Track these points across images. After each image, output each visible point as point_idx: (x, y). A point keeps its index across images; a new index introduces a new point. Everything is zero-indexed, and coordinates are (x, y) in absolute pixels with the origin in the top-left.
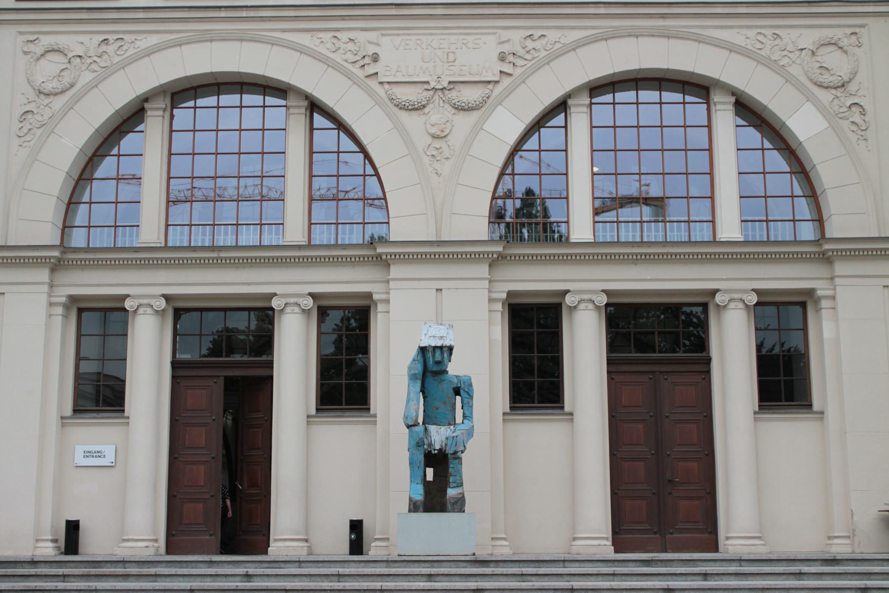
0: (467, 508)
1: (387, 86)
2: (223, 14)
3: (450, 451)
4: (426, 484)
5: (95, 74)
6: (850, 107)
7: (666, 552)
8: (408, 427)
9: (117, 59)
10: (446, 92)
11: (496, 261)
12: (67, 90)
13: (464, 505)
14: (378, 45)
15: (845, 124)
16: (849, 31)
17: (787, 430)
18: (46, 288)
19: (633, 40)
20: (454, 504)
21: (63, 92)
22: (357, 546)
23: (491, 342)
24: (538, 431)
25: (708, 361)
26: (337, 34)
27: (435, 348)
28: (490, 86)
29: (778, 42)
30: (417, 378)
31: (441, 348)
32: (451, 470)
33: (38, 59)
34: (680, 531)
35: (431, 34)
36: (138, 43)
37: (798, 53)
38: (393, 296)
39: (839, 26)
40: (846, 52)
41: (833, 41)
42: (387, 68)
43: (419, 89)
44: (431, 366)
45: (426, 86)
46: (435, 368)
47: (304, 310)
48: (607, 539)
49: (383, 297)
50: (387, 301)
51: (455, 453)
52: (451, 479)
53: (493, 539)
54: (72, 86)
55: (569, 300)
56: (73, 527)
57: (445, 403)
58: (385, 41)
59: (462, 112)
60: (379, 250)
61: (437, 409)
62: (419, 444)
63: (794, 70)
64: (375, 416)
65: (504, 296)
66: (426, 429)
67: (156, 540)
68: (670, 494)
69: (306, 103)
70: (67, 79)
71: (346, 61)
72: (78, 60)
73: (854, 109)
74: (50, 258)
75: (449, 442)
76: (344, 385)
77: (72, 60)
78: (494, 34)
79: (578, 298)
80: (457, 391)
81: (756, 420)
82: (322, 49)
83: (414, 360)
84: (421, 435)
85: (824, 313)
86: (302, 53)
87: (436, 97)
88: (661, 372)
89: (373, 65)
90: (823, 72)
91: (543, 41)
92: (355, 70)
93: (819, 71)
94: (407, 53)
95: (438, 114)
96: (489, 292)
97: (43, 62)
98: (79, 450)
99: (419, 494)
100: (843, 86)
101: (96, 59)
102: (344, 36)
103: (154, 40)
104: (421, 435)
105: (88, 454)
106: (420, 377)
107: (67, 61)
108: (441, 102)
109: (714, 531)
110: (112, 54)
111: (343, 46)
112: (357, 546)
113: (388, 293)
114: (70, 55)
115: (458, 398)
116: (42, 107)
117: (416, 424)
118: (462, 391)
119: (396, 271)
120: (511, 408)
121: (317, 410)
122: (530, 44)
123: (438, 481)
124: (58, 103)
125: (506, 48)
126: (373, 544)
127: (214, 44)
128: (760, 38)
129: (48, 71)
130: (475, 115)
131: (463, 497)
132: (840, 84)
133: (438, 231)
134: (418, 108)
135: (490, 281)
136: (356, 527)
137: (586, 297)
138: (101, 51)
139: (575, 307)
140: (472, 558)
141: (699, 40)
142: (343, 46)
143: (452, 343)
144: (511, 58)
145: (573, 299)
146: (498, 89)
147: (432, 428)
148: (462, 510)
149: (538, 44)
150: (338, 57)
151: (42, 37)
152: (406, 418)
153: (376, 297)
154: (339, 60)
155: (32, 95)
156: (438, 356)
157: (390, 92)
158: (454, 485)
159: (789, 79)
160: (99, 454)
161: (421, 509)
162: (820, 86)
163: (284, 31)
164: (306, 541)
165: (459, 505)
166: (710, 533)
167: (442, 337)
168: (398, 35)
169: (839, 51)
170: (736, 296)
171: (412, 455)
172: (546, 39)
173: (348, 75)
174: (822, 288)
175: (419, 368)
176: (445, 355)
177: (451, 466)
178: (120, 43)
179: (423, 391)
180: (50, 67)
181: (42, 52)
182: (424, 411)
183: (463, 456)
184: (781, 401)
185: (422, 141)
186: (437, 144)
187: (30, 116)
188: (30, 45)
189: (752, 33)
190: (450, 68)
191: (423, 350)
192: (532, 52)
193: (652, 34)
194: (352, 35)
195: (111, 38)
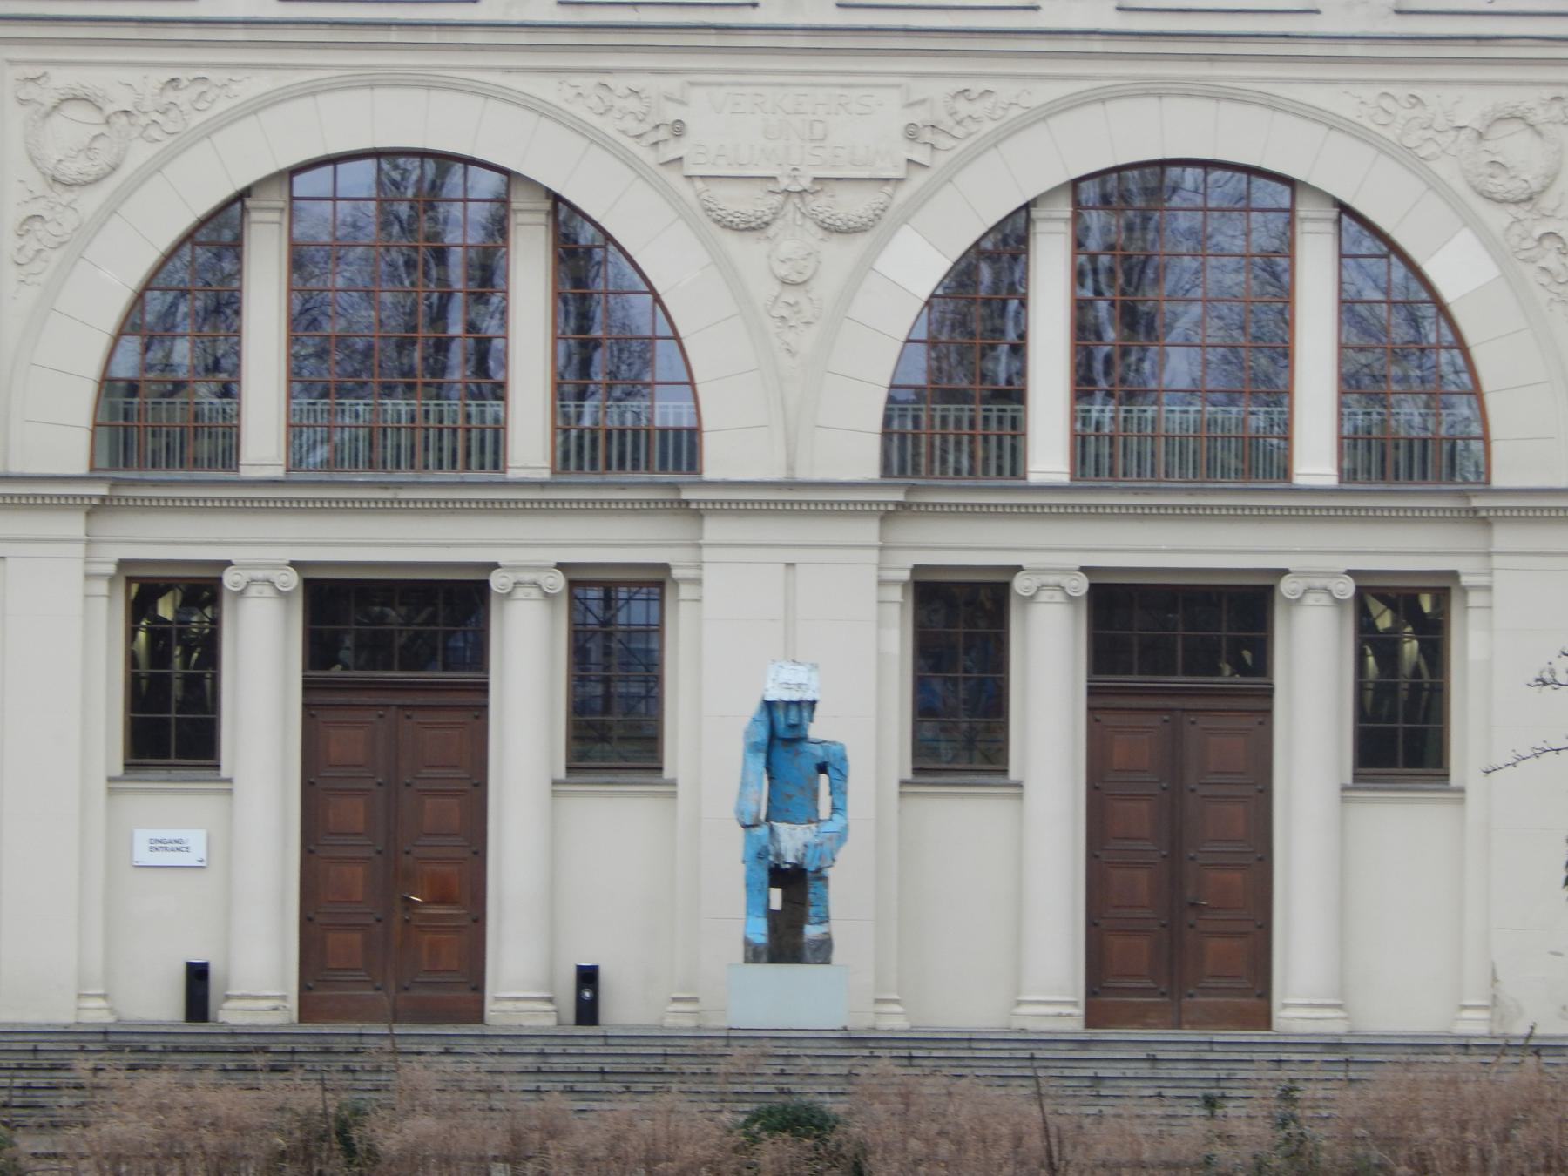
1: (699, 184)
2: (394, 36)
3: (811, 867)
4: (772, 916)
5: (157, 147)
6: (1541, 239)
7: (1180, 1027)
8: (745, 827)
9: (197, 119)
10: (809, 198)
12: (106, 176)
14: (682, 103)
15: (1530, 271)
16: (1548, 93)
17: (1400, 818)
18: (80, 549)
19: (1153, 101)
21: (97, 180)
22: (587, 1012)
23: (881, 656)
24: (961, 816)
25: (1268, 694)
26: (607, 79)
27: (789, 704)
28: (888, 189)
29: (1417, 111)
30: (759, 750)
31: (799, 704)
32: (811, 896)
33: (48, 115)
34: (1206, 991)
35: (782, 85)
36: (235, 87)
37: (1453, 133)
39: (1533, 84)
40: (1539, 134)
41: (1518, 114)
42: (702, 150)
43: (756, 190)
44: (783, 735)
45: (771, 186)
46: (789, 735)
47: (546, 595)
48: (1074, 1004)
49: (691, 573)
50: (698, 582)
51: (819, 870)
52: (812, 910)
53: (878, 1001)
54: (114, 169)
56: (588, 977)
57: (802, 788)
58: (697, 94)
59: (836, 236)
61: (790, 797)
62: (761, 855)
63: (1442, 168)
64: (673, 783)
66: (772, 829)
67: (283, 998)
68: (1192, 926)
69: (547, 205)
70: (103, 160)
71: (624, 132)
72: (124, 119)
73: (1547, 243)
74: (90, 497)
76: (615, 723)
77: (113, 119)
78: (898, 86)
80: (822, 768)
81: (1344, 800)
82: (579, 110)
83: (755, 720)
84: (765, 841)
85: (1473, 615)
86: (542, 114)
87: (790, 207)
88: (1184, 710)
89: (672, 143)
90: (1497, 171)
91: (988, 102)
92: (641, 150)
93: (1489, 171)
94: (739, 119)
95: (793, 241)
97: (56, 120)
98: (142, 837)
99: (759, 932)
100: (1530, 199)
101: (156, 116)
102: (619, 84)
103: (262, 83)
104: (765, 841)
105: (157, 845)
106: (764, 748)
107: (102, 120)
108: (798, 216)
109: (1265, 993)
110: (186, 107)
111: (619, 103)
112: (587, 1012)
113: (700, 567)
114: (109, 109)
115: (824, 778)
116: (59, 208)
118: (830, 769)
121: (569, 769)
122: (963, 107)
123: (791, 919)
124: (91, 201)
125: (920, 116)
127: (378, 92)
128: (1386, 103)
129: (67, 136)
130: (860, 243)
132: (1523, 197)
133: (791, 467)
134: (756, 227)
136: (197, 975)
137: (1051, 579)
138: (165, 100)
140: (844, 1034)
141: (1273, 104)
142: (619, 103)
144: (927, 135)
145: (1027, 583)
146: (903, 194)
147: (782, 828)
148: (826, 961)
149: (978, 108)
150: (608, 126)
151: (52, 71)
152: (740, 813)
153: (677, 573)
154: (610, 131)
155: (39, 186)
156: (793, 717)
157: (705, 196)
159: (1435, 185)
160: (178, 846)
161: (765, 958)
162: (1490, 197)
163: (508, 70)
165: (823, 951)
166: (1259, 996)
167: (799, 685)
168: (720, 85)
169: (1528, 133)
170: (1317, 582)
171: (750, 870)
172: (992, 99)
173: (629, 161)
174: (1469, 570)
175: (762, 734)
178: (201, 88)
179: (769, 767)
180: (72, 128)
181: (55, 101)
182: (770, 800)
183: (831, 873)
184: (1395, 766)
185: (764, 289)
186: (790, 296)
187: (37, 225)
188: (31, 87)
189: (1370, 94)
190: (816, 152)
191: (769, 706)
192: (968, 122)
193: (1189, 91)
194: (636, 82)
195: (184, 75)
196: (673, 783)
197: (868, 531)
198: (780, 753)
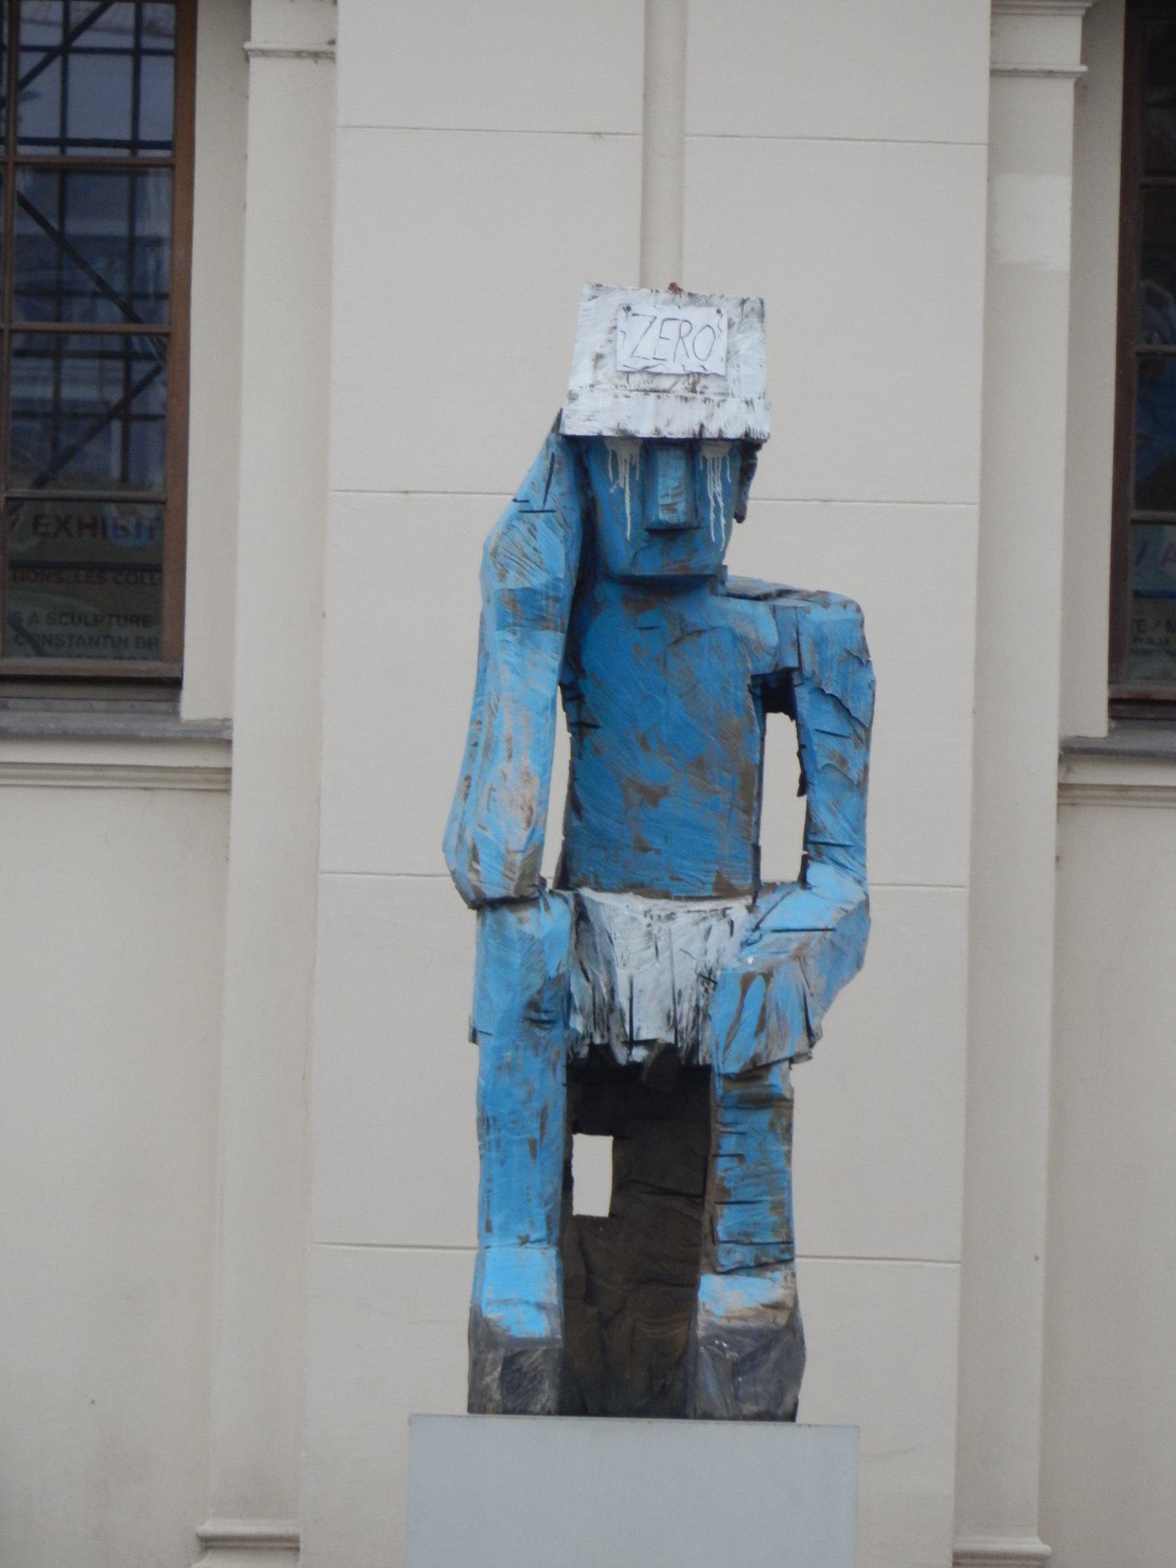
0: (814, 1391)
4: (575, 1238)
44: (630, 562)
52: (727, 1221)
62: (542, 1011)
64: (218, 737)
80: (775, 692)
106: (560, 611)
115: (779, 726)
120: (1125, 708)
133: (501, 924)
147: (620, 912)
158: (741, 1254)
161: (547, 1393)
165: (765, 1375)
171: (499, 1069)
175: (552, 560)
176: (715, 488)
177: (729, 1144)
183: (801, 1082)
191: (580, 456)
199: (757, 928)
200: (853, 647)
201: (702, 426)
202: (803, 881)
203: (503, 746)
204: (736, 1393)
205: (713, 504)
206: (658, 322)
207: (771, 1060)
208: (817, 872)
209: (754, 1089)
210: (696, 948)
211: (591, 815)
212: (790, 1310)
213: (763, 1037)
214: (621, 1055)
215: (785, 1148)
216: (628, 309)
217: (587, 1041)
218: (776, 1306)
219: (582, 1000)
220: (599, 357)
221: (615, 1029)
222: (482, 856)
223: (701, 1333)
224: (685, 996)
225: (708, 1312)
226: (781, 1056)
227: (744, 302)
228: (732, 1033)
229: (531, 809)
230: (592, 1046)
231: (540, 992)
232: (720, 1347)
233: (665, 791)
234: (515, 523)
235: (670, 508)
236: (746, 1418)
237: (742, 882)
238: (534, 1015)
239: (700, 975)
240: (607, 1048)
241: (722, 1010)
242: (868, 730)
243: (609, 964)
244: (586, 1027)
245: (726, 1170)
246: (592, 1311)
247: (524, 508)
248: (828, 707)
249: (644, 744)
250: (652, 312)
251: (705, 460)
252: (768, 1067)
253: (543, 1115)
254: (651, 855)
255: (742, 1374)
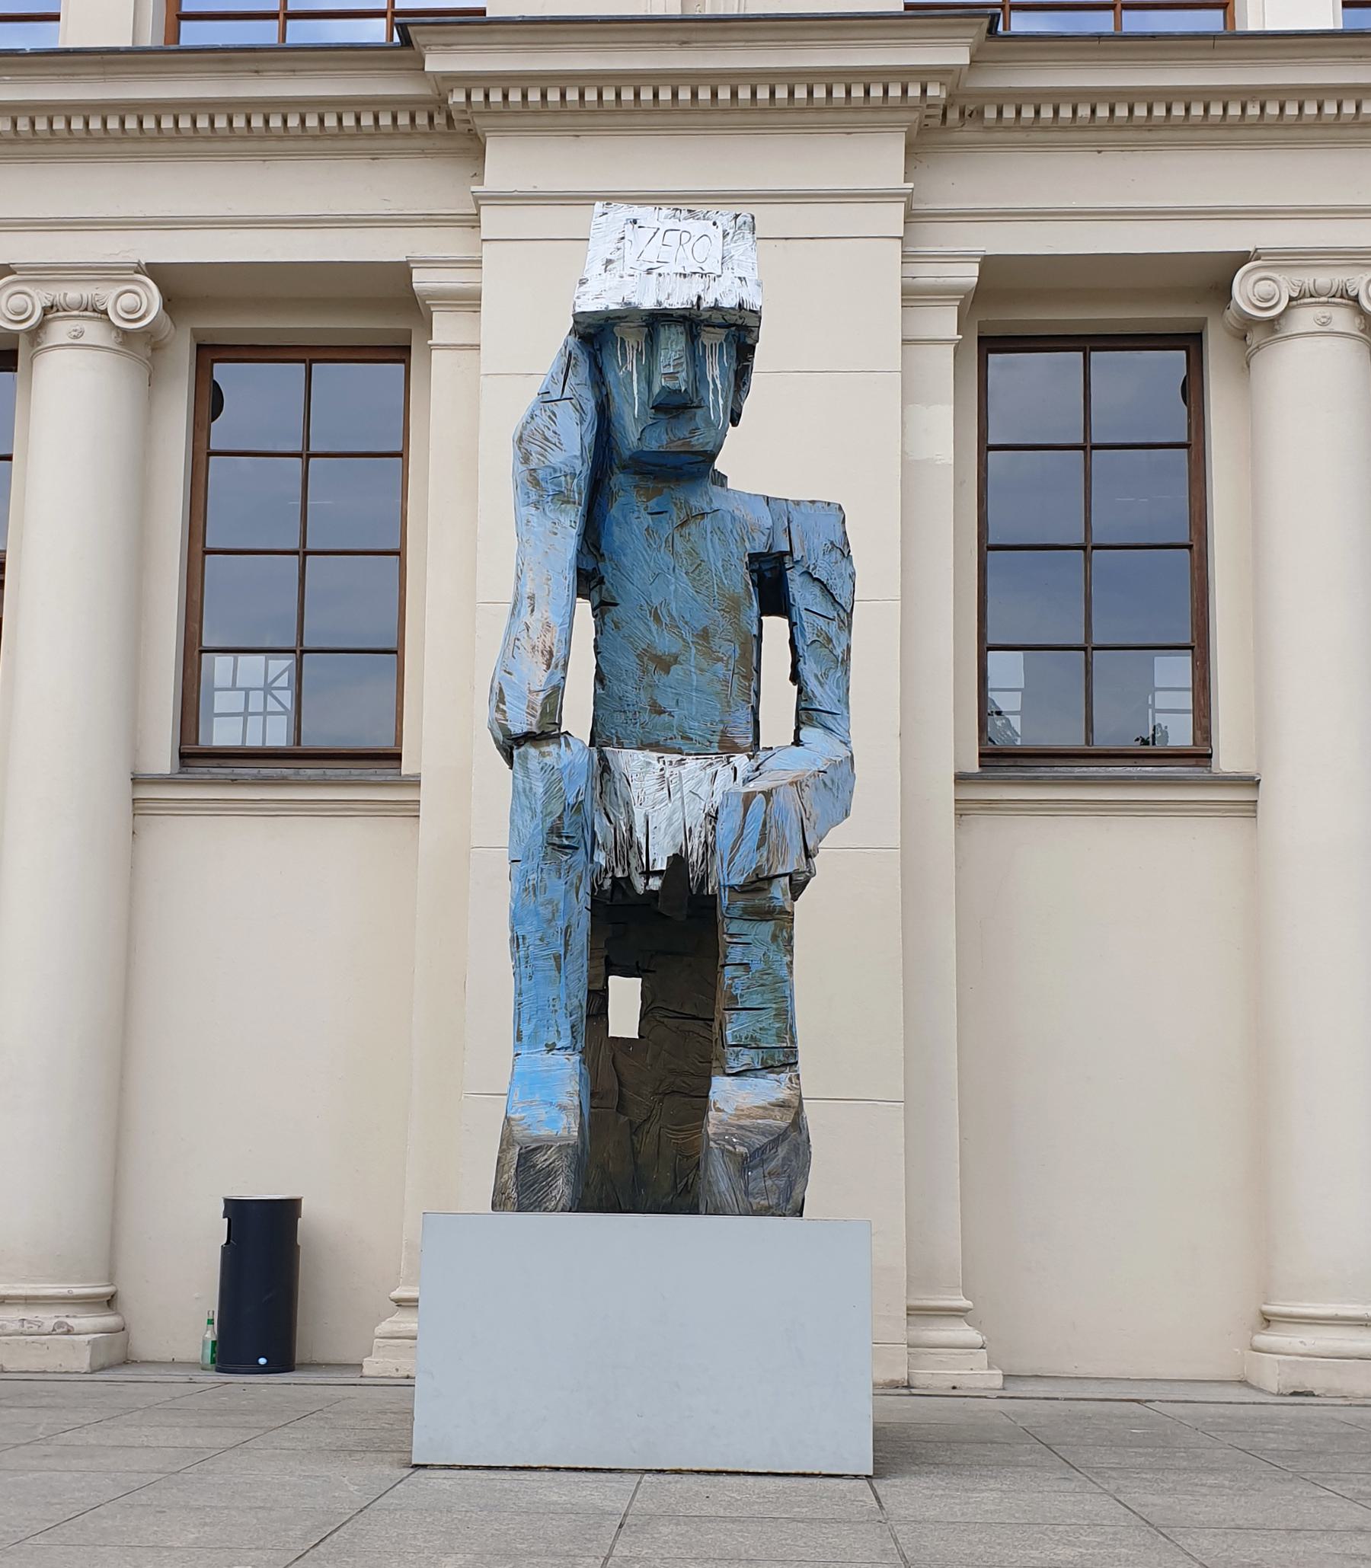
0: (814, 1193)
3: (727, 874)
11: (943, 125)
13: (804, 1170)
20: (745, 1164)
23: (909, 467)
27: (657, 320)
30: (562, 497)
38: (491, 283)
50: (469, 301)
52: (735, 1027)
53: (913, 1312)
55: (1248, 291)
60: (434, 63)
62: (562, 839)
65: (968, 274)
66: (605, 767)
75: (726, 828)
79: (1285, 284)
80: (771, 582)
96: (907, 258)
99: (557, 1114)
106: (578, 488)
115: (776, 629)
117: (547, 733)
119: (509, 163)
126: (384, 1327)
131: (798, 1124)
135: (911, 217)
137: (1325, 279)
139: (1272, 326)
143: (754, 299)
147: (630, 761)
158: (747, 1058)
161: (561, 1188)
164: (110, 1302)
165: (775, 1176)
171: (528, 890)
175: (571, 441)
176: (714, 371)
177: (735, 954)
179: (590, 579)
182: (600, 678)
191: (595, 336)
196: (415, 782)
197: (881, 160)
198: (633, 518)
199: (757, 769)
200: (837, 539)
201: (699, 298)
202: (797, 742)
203: (526, 602)
204: (746, 1187)
205: (711, 386)
206: (660, 233)
207: (772, 873)
208: (806, 733)
209: (758, 900)
210: (704, 790)
211: (616, 688)
212: (794, 1109)
213: (764, 851)
214: (639, 884)
215: (788, 958)
216: (635, 222)
217: (610, 875)
218: (783, 1105)
219: (605, 838)
220: (609, 262)
221: (634, 863)
222: (507, 699)
223: (711, 1130)
224: (696, 833)
225: (718, 1110)
226: (780, 871)
227: (737, 216)
228: (735, 847)
229: (551, 653)
230: (613, 877)
231: (560, 818)
232: (729, 1142)
233: (676, 660)
234: (537, 412)
235: (672, 376)
236: (756, 1213)
237: (744, 740)
238: (556, 840)
239: (708, 815)
240: (628, 879)
241: (726, 828)
242: (850, 615)
243: (627, 804)
244: (608, 861)
245: (733, 978)
246: (623, 1119)
247: (545, 398)
248: (817, 590)
249: (657, 618)
250: (657, 225)
251: (704, 346)
252: (770, 879)
253: (567, 932)
254: (665, 716)
255: (751, 1169)
